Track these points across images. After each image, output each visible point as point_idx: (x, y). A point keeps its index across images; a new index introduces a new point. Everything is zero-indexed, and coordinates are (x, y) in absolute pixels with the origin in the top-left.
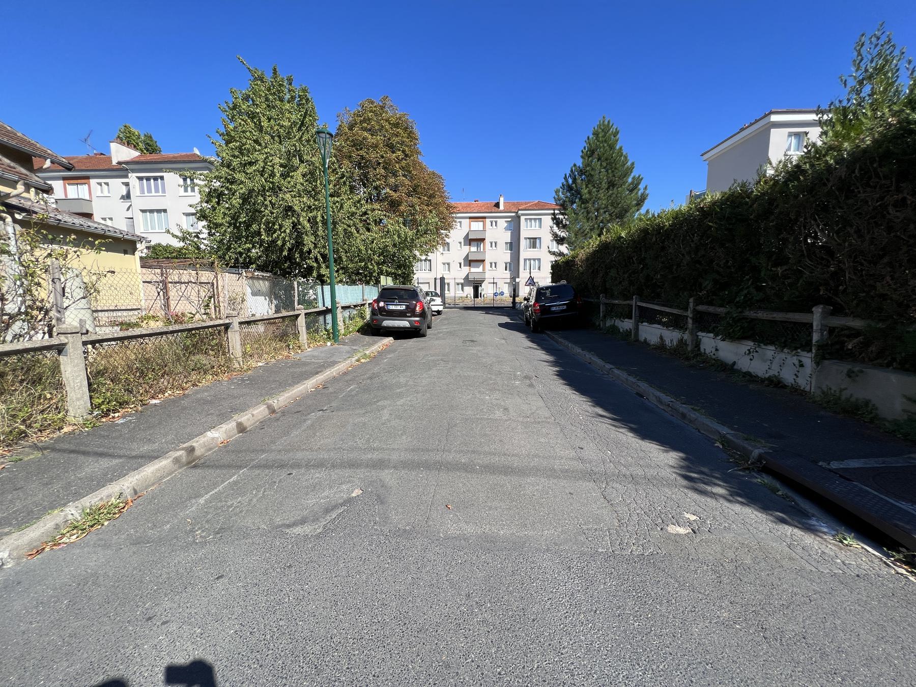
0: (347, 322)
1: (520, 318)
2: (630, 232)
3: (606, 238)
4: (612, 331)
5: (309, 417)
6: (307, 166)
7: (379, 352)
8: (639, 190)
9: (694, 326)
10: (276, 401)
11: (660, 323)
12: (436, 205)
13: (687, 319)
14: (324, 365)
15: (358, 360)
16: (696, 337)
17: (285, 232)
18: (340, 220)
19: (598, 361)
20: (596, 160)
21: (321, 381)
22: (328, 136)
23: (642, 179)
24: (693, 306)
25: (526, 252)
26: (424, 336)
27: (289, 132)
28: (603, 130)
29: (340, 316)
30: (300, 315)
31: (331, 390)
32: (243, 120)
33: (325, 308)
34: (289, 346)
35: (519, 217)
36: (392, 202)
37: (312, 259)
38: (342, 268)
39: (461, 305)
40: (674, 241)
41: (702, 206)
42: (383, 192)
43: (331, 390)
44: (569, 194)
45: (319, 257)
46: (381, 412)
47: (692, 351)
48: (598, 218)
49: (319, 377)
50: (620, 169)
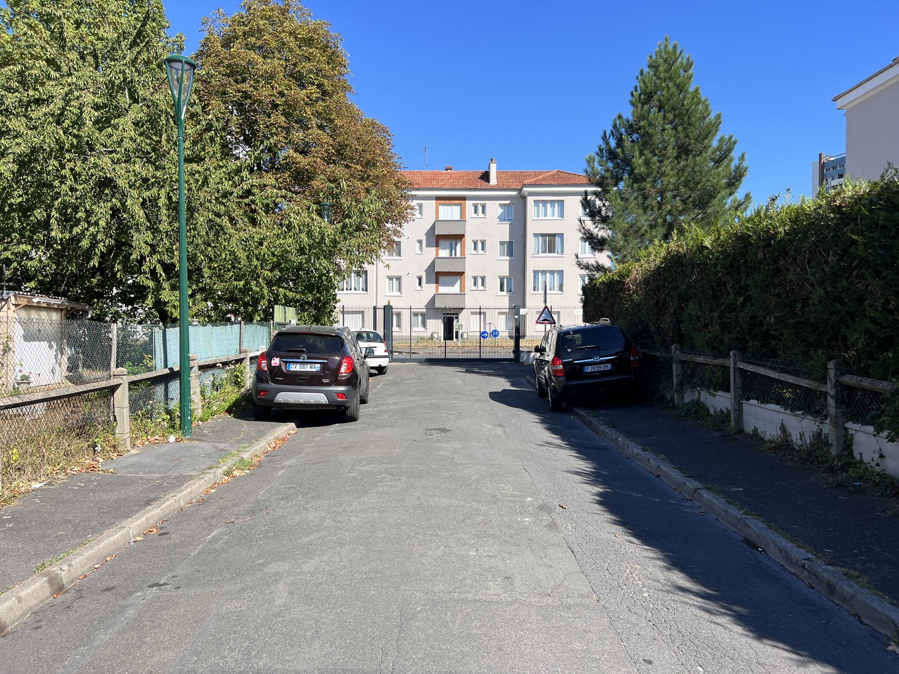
0: (208, 394)
1: (529, 382)
2: (718, 238)
3: (678, 246)
4: (696, 412)
5: (131, 600)
6: (145, 108)
7: (267, 455)
8: (731, 160)
9: (840, 410)
10: (65, 567)
11: (779, 400)
12: (378, 181)
13: (826, 399)
14: (160, 485)
15: (228, 473)
16: (843, 431)
17: (96, 224)
18: (201, 205)
19: (672, 474)
20: (655, 110)
21: (156, 519)
22: (186, 67)
23: (735, 142)
24: (836, 375)
25: (536, 260)
26: (353, 419)
27: (113, 49)
28: (665, 61)
29: (196, 381)
30: (118, 386)
31: (175, 538)
32: (30, 26)
33: (167, 371)
34: (94, 446)
35: (524, 198)
36: (298, 173)
37: (145, 273)
38: (202, 290)
39: (423, 355)
40: (795, 260)
41: (838, 203)
42: (282, 154)
43: (175, 538)
44: (610, 165)
45: (159, 270)
46: (273, 588)
47: (839, 456)
48: (664, 207)
49: (153, 512)
50: (697, 124)
